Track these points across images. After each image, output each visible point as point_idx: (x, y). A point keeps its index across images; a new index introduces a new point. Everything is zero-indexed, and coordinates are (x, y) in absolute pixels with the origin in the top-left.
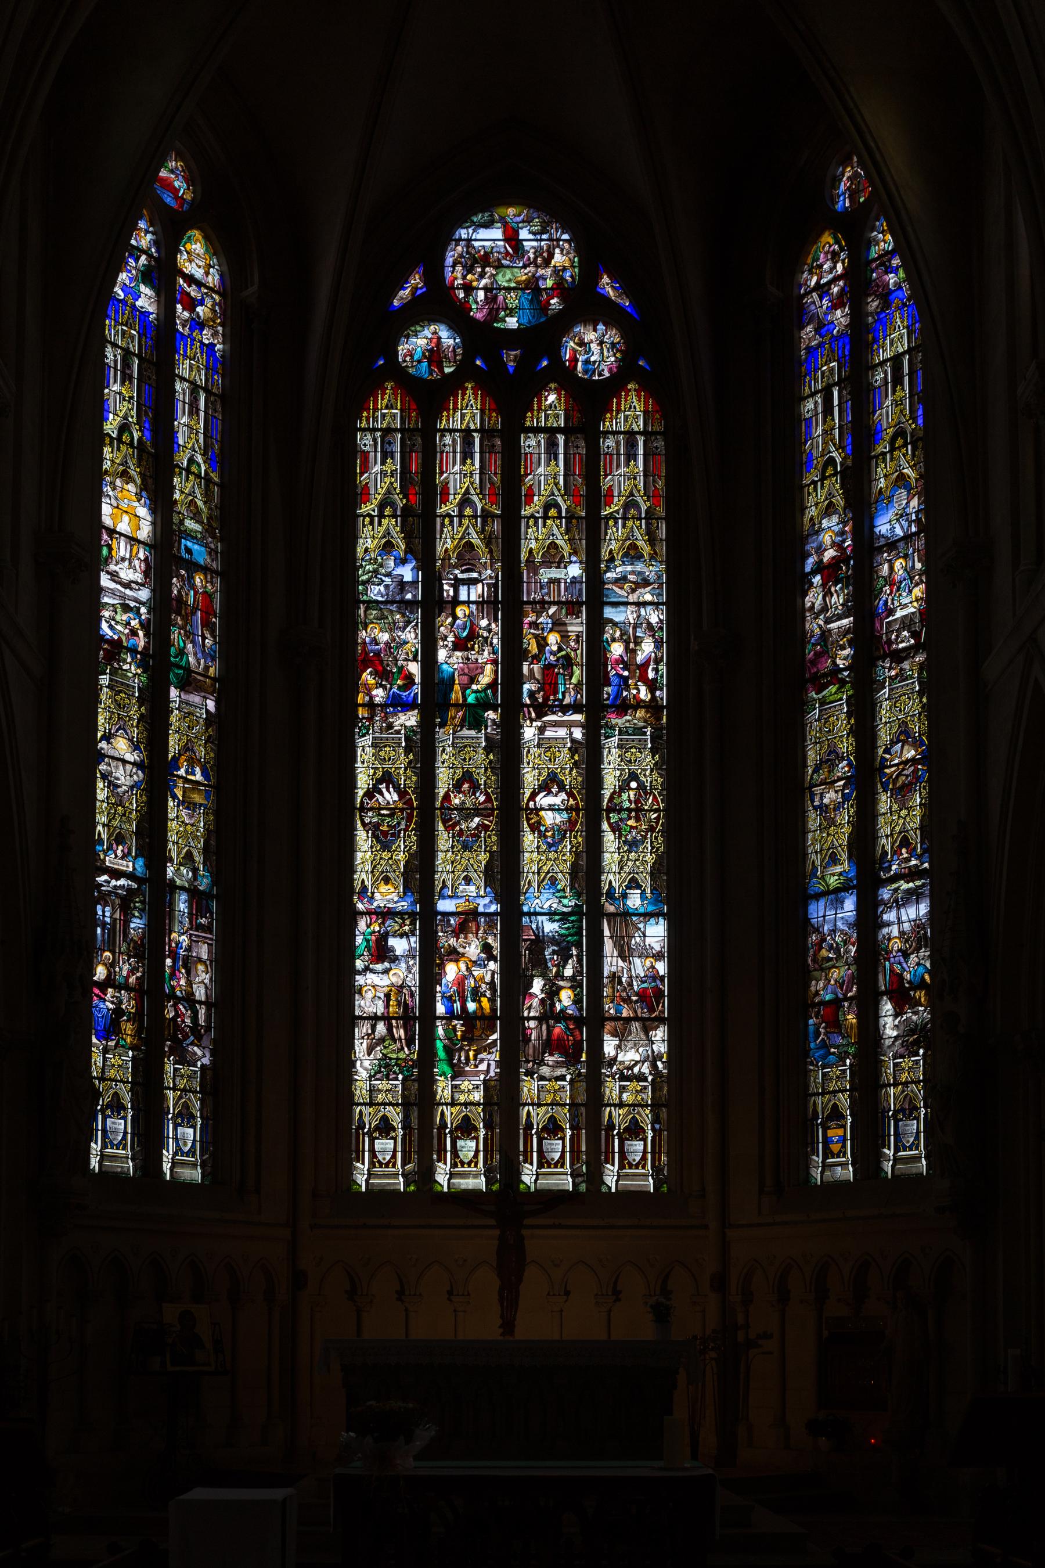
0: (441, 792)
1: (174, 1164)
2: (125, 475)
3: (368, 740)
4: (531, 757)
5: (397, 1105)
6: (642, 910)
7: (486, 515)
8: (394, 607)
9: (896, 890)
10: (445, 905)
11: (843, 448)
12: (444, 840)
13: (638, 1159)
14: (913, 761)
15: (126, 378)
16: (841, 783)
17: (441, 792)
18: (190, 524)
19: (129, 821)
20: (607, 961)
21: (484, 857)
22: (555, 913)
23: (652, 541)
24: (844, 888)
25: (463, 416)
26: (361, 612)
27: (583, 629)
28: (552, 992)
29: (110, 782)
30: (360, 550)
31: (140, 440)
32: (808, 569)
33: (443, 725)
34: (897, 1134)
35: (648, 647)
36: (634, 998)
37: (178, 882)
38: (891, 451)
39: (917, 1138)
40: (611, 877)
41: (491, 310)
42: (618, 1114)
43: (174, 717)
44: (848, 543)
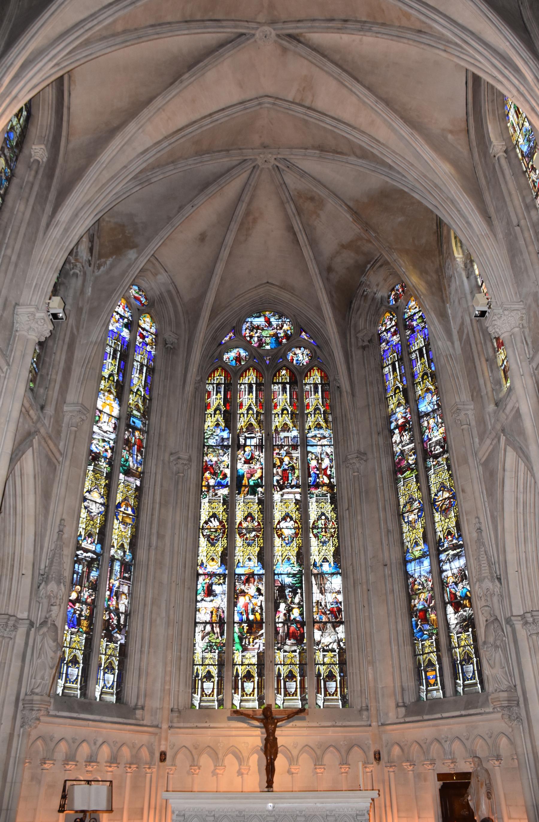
0: (238, 521)
1: (102, 693)
2: (110, 392)
3: (207, 500)
4: (278, 507)
5: (215, 665)
6: (329, 572)
7: (258, 413)
8: (219, 448)
9: (448, 555)
10: (238, 571)
11: (402, 382)
12: (239, 541)
13: (333, 691)
14: (449, 498)
15: (114, 357)
16: (417, 511)
17: (238, 521)
18: (135, 412)
19: (95, 528)
20: (314, 595)
21: (257, 549)
22: (290, 574)
23: (326, 421)
24: (424, 555)
25: (249, 379)
26: (206, 449)
27: (299, 455)
28: (289, 610)
29: (88, 511)
30: (206, 427)
31: (117, 380)
32: (392, 428)
33: (239, 494)
34: (463, 673)
35: (326, 463)
36: (328, 612)
37: (116, 557)
38: (422, 381)
39: (474, 673)
40: (315, 557)
41: (260, 344)
42: (323, 669)
43: (121, 486)
44: (409, 415)
